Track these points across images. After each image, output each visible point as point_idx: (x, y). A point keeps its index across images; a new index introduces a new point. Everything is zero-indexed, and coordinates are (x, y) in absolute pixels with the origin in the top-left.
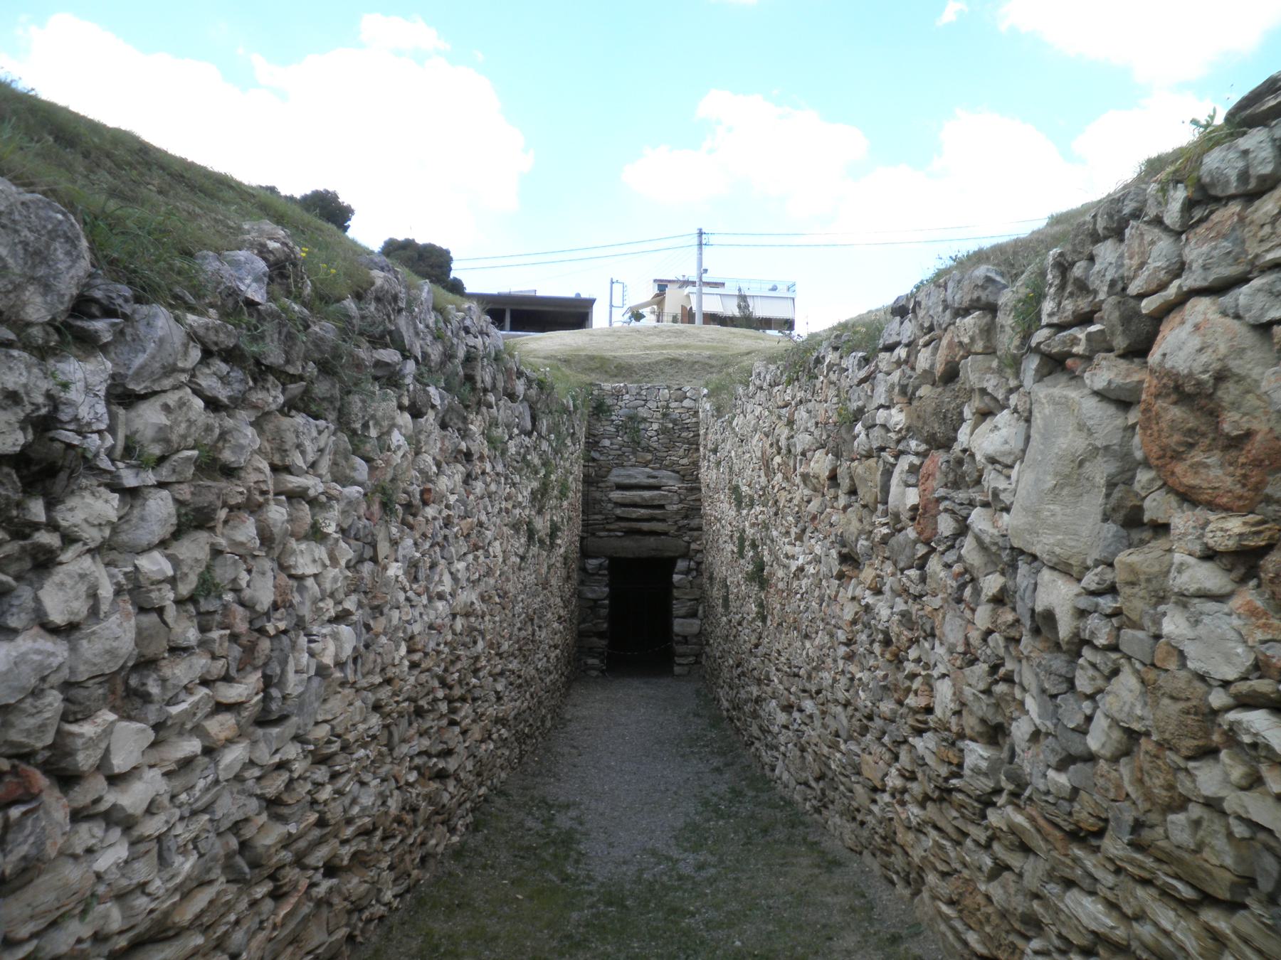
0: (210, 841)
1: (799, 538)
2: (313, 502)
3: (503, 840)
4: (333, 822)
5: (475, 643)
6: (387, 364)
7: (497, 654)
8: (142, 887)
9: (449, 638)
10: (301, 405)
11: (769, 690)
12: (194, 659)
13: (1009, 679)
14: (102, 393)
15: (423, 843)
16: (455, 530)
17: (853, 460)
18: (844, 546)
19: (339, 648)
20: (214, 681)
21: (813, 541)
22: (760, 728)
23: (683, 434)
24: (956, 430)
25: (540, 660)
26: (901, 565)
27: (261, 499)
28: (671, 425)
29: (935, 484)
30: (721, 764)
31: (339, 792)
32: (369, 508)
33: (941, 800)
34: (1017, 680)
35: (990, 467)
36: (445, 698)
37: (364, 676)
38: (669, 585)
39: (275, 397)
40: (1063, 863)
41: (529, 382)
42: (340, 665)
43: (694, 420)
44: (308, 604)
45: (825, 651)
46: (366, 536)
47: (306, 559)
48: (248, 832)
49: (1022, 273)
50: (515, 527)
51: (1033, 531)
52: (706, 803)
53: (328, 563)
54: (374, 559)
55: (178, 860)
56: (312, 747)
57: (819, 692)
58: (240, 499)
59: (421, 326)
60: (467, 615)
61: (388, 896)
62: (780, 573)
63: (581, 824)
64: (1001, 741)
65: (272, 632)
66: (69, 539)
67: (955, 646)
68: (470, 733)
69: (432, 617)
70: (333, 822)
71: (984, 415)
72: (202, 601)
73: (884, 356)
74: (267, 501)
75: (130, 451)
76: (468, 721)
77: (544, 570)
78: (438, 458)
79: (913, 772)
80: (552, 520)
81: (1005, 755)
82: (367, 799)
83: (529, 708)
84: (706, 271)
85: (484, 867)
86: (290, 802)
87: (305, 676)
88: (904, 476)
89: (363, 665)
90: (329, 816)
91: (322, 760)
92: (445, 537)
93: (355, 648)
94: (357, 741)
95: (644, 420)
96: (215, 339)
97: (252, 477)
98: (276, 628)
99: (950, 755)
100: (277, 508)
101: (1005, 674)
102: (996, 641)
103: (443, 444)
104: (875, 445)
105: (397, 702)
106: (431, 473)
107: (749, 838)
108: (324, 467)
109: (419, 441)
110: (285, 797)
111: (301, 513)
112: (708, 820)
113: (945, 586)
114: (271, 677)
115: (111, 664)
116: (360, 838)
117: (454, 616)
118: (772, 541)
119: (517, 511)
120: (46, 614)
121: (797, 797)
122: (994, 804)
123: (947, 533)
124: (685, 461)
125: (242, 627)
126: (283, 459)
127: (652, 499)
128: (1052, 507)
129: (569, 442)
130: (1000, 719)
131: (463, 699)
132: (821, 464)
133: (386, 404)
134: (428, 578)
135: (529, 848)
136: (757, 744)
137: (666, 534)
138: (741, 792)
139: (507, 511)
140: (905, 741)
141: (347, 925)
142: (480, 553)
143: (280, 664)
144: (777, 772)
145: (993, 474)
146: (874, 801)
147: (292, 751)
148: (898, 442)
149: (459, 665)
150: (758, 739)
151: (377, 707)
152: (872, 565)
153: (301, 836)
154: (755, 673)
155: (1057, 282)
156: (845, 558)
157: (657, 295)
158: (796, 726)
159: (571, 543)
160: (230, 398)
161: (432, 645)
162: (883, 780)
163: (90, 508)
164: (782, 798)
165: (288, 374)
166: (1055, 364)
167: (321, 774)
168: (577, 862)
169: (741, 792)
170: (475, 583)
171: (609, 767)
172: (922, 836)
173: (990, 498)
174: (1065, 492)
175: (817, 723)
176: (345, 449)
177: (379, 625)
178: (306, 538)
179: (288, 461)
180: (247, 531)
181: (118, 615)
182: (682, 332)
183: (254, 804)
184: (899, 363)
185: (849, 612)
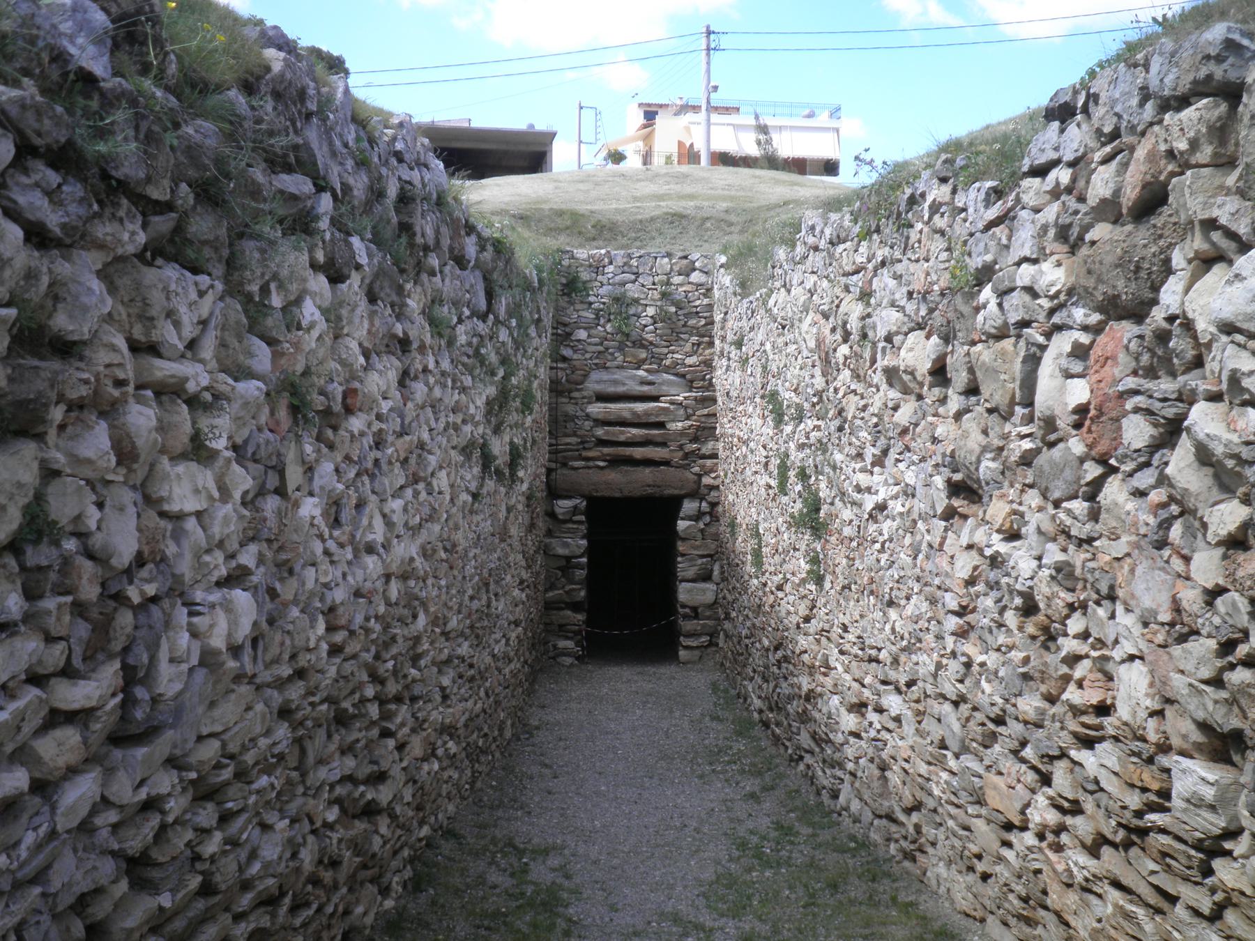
0: (43, 927)
1: (879, 461)
2: (193, 402)
3: (457, 903)
4: (223, 887)
5: (415, 617)
6: (294, 198)
7: (443, 633)
9: (382, 609)
10: (170, 249)
11: (828, 682)
12: (18, 642)
15: (347, 912)
16: (390, 451)
17: (973, 343)
18: (955, 471)
19: (233, 624)
20: (48, 677)
21: (902, 466)
22: (814, 736)
23: (689, 322)
24: (1156, 289)
25: (497, 642)
26: (1057, 495)
27: (116, 393)
28: (673, 309)
29: (1117, 372)
30: (757, 789)
31: (234, 843)
32: (272, 413)
33: (1127, 845)
35: (1224, 338)
36: (375, 698)
38: (673, 535)
39: (133, 233)
41: (482, 243)
42: (235, 650)
43: (706, 301)
44: (188, 556)
45: (923, 624)
46: (270, 457)
47: (185, 488)
48: (100, 910)
50: (466, 450)
52: (743, 845)
53: (216, 495)
54: (281, 491)
56: (193, 775)
57: (910, 684)
58: (84, 391)
59: (338, 143)
60: (404, 577)
62: (847, 514)
64: (1236, 758)
65: (136, 599)
67: (1155, 613)
68: (408, 749)
69: (360, 578)
70: (223, 887)
71: (1206, 262)
72: (29, 551)
73: (1032, 184)
74: (123, 400)
76: (406, 730)
77: (502, 514)
78: (366, 344)
79: (1075, 802)
80: (511, 443)
82: (271, 850)
83: (484, 711)
84: (716, 88)
86: (161, 859)
87: (184, 667)
88: (1064, 362)
89: (265, 649)
90: (218, 878)
91: (205, 792)
92: (377, 462)
93: (255, 624)
94: (257, 763)
95: (636, 301)
96: (36, 125)
97: (103, 357)
98: (142, 593)
99: (1146, 776)
100: (138, 407)
101: (1248, 655)
102: (1234, 604)
103: (372, 324)
104: (1013, 318)
105: (312, 704)
106: (357, 366)
107: (812, 896)
108: (208, 349)
109: (339, 318)
110: (155, 854)
111: (176, 418)
112: (749, 870)
113: (1135, 524)
114: (135, 668)
116: (262, 909)
117: (388, 577)
118: (834, 468)
119: (468, 429)
121: (875, 836)
123: (1139, 444)
124: (690, 361)
125: (90, 591)
126: (147, 333)
127: (647, 413)
129: (532, 331)
130: (1235, 722)
131: (398, 699)
132: (918, 353)
133: (293, 259)
134: (355, 523)
135: (496, 914)
136: (808, 759)
137: (667, 463)
138: (790, 828)
139: (456, 428)
140: (1063, 755)
142: (421, 486)
143: (148, 648)
144: (842, 799)
145: (1231, 349)
146: (1007, 844)
147: (165, 782)
148: (1052, 312)
149: (394, 650)
150: (811, 752)
151: (285, 713)
152: (1003, 496)
153: (176, 913)
154: (805, 657)
156: (955, 489)
157: (645, 126)
158: (873, 734)
159: (536, 476)
160: (63, 226)
161: (359, 619)
162: (1023, 812)
164: (853, 838)
165: (148, 200)
167: (207, 815)
169: (790, 828)
170: (414, 530)
171: (598, 793)
172: (1091, 897)
173: (1224, 386)
175: (909, 728)
176: (238, 323)
177: (287, 590)
178: (183, 456)
179: (155, 336)
180: (96, 442)
182: (686, 176)
183: (108, 867)
184: (1056, 193)
185: (964, 566)
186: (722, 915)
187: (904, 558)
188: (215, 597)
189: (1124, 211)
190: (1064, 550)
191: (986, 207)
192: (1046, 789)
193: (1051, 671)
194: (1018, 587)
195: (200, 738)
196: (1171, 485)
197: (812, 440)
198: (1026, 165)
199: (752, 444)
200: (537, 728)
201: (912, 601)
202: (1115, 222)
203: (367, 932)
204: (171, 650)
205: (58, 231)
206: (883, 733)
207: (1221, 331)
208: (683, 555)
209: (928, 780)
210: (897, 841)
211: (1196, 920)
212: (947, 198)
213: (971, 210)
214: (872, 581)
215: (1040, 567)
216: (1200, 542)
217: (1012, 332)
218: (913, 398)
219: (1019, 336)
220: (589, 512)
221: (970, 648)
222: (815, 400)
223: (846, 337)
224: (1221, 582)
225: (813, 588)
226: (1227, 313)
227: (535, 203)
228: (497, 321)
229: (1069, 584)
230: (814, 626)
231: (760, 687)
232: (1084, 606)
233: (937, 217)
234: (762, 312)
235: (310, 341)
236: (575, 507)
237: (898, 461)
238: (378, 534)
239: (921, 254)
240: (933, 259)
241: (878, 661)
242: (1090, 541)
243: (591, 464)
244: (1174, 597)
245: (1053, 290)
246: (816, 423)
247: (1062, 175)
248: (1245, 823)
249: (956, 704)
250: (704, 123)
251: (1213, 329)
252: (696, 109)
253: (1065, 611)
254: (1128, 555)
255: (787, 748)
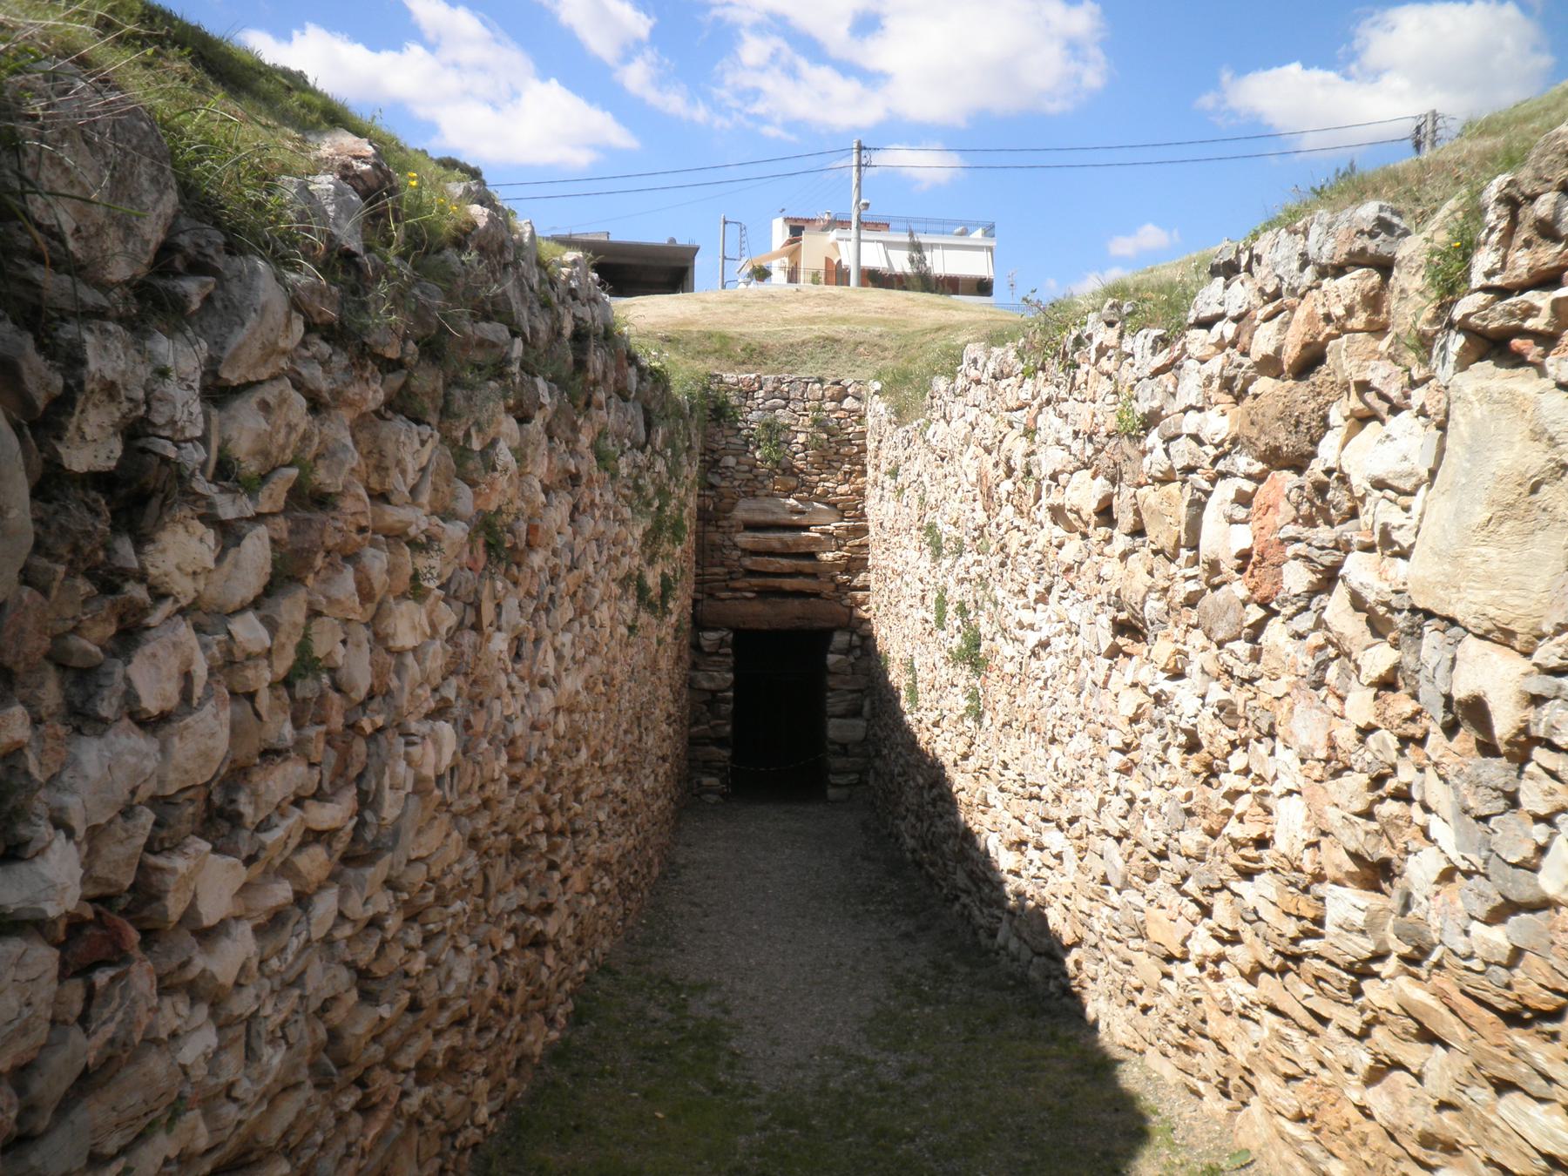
1: (1042, 599)
2: (414, 544)
5: (578, 750)
6: (494, 345)
8: (228, 1092)
9: (551, 742)
13: (1403, 796)
14: (196, 385)
15: (519, 1040)
17: (1140, 486)
22: (971, 875)
23: (840, 450)
24: (1314, 443)
25: (647, 777)
26: (1220, 636)
27: (359, 538)
32: (471, 552)
33: (1283, 971)
34: (1416, 795)
35: (1377, 493)
37: (461, 796)
40: (1496, 1057)
43: (858, 428)
45: (1086, 761)
48: (337, 1015)
49: (1434, 211)
50: (623, 582)
51: (1451, 584)
52: (900, 983)
54: (477, 627)
55: (267, 1051)
56: (405, 896)
57: (1072, 821)
60: (570, 711)
61: (483, 1114)
62: (1008, 650)
63: (727, 1012)
64: (1385, 886)
65: (369, 729)
66: (159, 596)
68: (570, 882)
71: (1362, 419)
72: (298, 683)
75: (224, 470)
76: (569, 863)
79: (1235, 933)
80: (663, 575)
81: (1395, 902)
82: (462, 974)
85: (601, 1074)
86: (380, 974)
87: (402, 793)
88: (1228, 508)
89: (460, 780)
90: (423, 995)
93: (455, 753)
94: (453, 888)
99: (1301, 905)
101: (1397, 789)
102: (1384, 742)
103: (550, 462)
104: (1179, 464)
105: (495, 834)
109: (524, 456)
112: (909, 1007)
113: (1294, 665)
114: (367, 793)
115: (204, 772)
116: (456, 1029)
119: (626, 561)
120: (137, 699)
121: (1033, 974)
122: (1376, 975)
124: (842, 489)
128: (1483, 550)
129: (684, 458)
130: (1384, 851)
131: (561, 833)
132: (1085, 493)
134: (534, 662)
136: (964, 899)
137: (817, 595)
141: (439, 1155)
142: (585, 619)
144: (1000, 938)
145: (1383, 504)
146: (1167, 976)
150: (968, 893)
153: (394, 1023)
155: (1503, 224)
156: (1121, 628)
157: (791, 242)
158: (1033, 871)
159: (684, 608)
162: (1184, 944)
163: (181, 551)
164: (1011, 976)
166: (1493, 346)
168: (731, 1066)
172: (1249, 1023)
173: (1376, 538)
174: (1505, 528)
177: (478, 722)
180: (345, 584)
181: (213, 702)
183: (345, 976)
184: (1221, 346)
185: (1130, 702)
186: (884, 1049)
187: (1068, 697)
188: (425, 728)
189: (1286, 368)
190: (1227, 689)
191: (1153, 354)
192: (1206, 920)
193: (1213, 806)
194: (1183, 725)
195: (410, 862)
196: (1328, 629)
197: (973, 575)
198: (1192, 317)
199: (907, 578)
200: (684, 867)
201: (1075, 738)
202: (1277, 377)
203: (536, 1060)
204: (391, 777)
205: (327, 396)
206: (1044, 870)
207: (1374, 487)
208: (832, 690)
209: (1090, 916)
210: (1056, 978)
211: (1347, 1039)
212: (1114, 342)
213: (1138, 356)
214: (1034, 718)
215: (1203, 705)
216: (1354, 683)
217: (1178, 477)
218: (1078, 535)
219: (1184, 482)
220: (736, 645)
221: (1134, 784)
222: (976, 534)
223: (1010, 472)
224: (1373, 721)
225: (972, 724)
226: (1380, 472)
227: (684, 324)
228: (654, 452)
229: (1231, 722)
230: (972, 764)
231: (913, 826)
232: (1245, 743)
233: (1104, 360)
234: (920, 442)
235: (502, 482)
236: (722, 639)
237: (1062, 598)
238: (549, 666)
239: (1088, 394)
240: (1099, 401)
241: (1039, 799)
242: (1251, 681)
243: (738, 595)
244: (1329, 734)
245: (1217, 440)
246: (976, 557)
247: (1227, 329)
248: (1391, 946)
249: (1119, 840)
250: (854, 241)
251: (1369, 486)
252: (844, 224)
253: (1228, 748)
254: (1288, 694)
255: (941, 888)
